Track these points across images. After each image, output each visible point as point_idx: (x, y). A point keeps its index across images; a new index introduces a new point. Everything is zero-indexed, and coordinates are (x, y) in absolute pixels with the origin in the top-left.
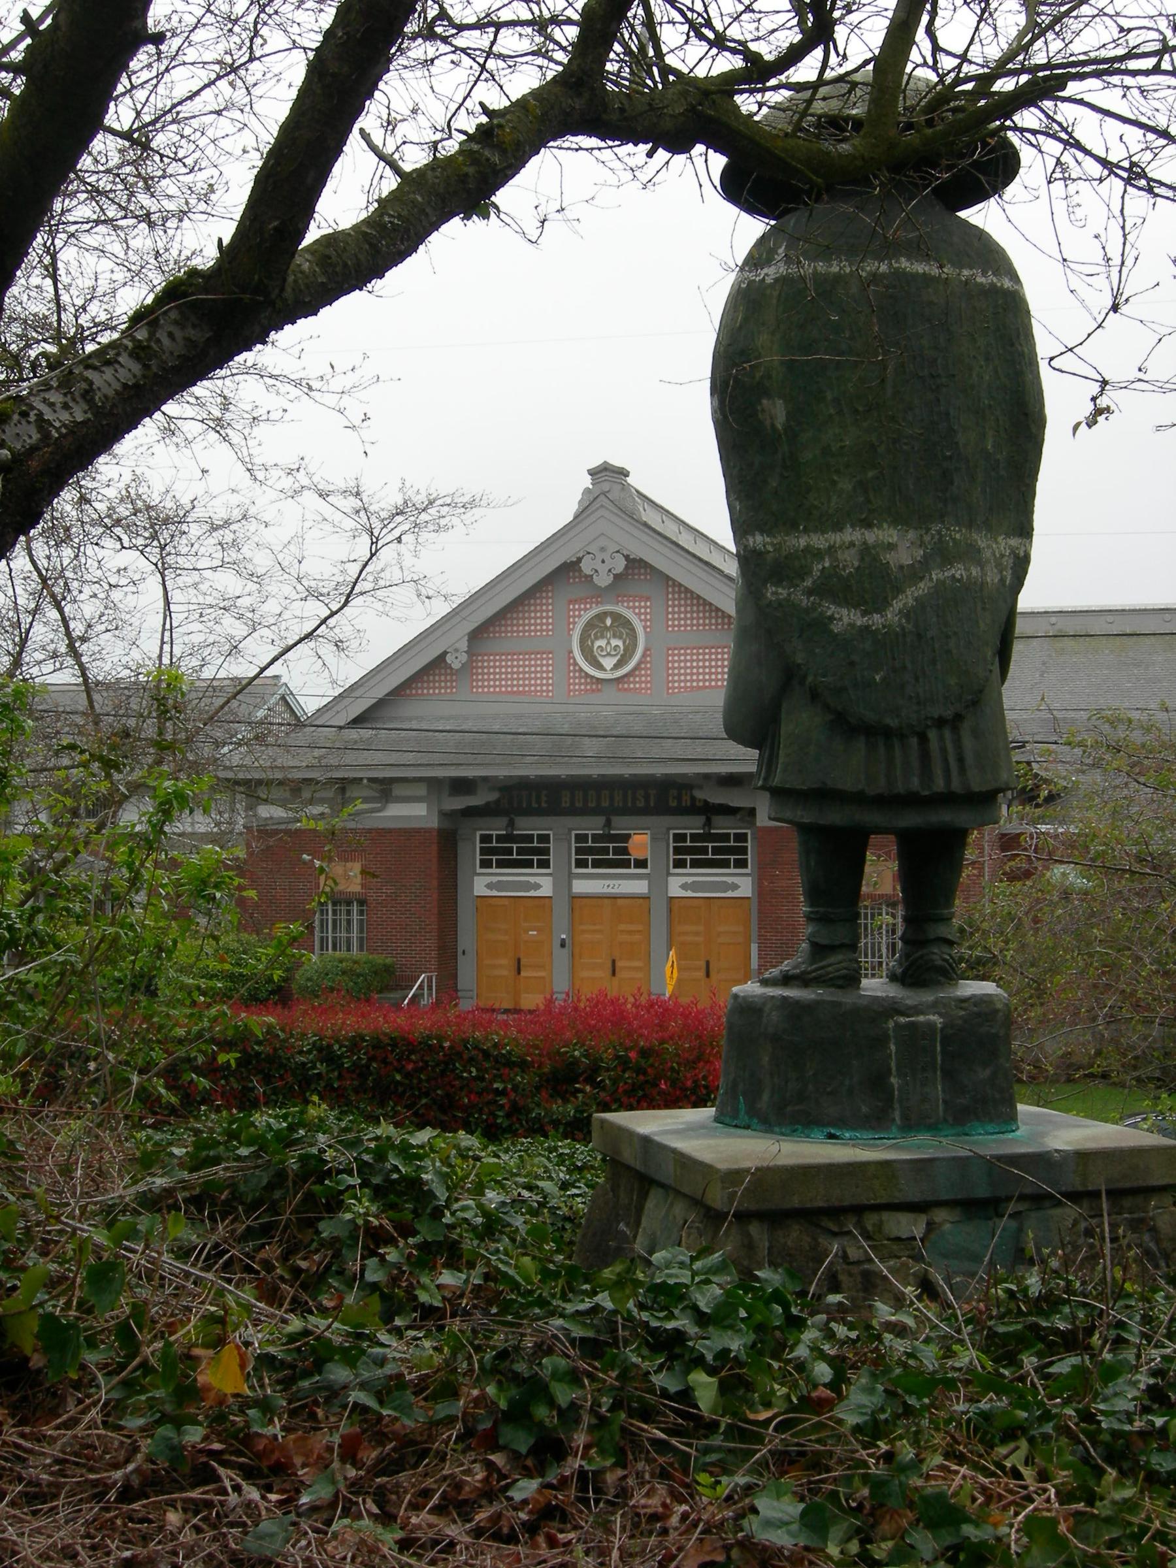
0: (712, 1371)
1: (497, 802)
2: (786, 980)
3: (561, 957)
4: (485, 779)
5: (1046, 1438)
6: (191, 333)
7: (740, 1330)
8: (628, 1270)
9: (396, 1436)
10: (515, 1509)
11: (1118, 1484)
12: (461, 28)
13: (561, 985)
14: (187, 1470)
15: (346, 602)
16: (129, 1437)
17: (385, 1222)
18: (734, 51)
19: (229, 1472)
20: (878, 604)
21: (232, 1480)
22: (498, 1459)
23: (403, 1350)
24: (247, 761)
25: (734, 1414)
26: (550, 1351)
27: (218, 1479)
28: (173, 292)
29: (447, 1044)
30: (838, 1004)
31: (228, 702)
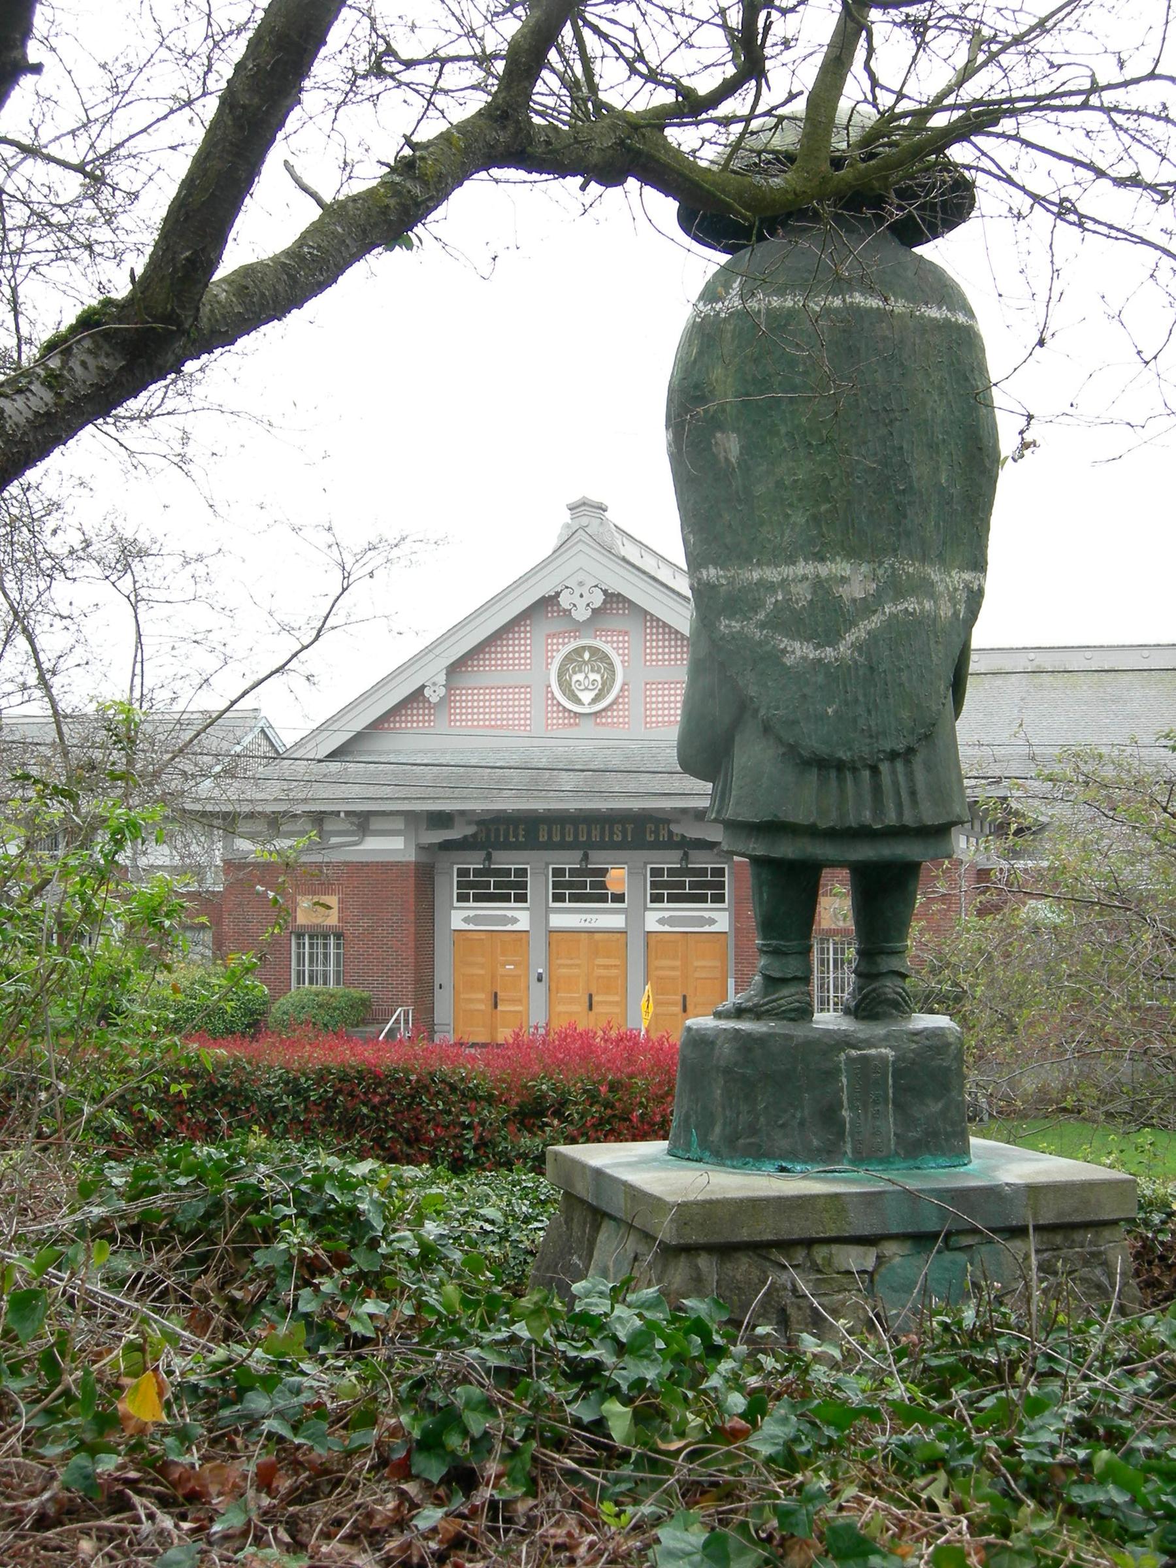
0: (627, 1401)
1: (474, 836)
2: (739, 1012)
3: (538, 992)
4: (462, 813)
5: (968, 1471)
6: (106, 362)
7: (655, 1360)
8: (546, 1300)
9: (311, 1466)
10: (426, 1538)
11: (1036, 1516)
12: (409, 64)
13: (537, 1017)
14: (100, 1498)
15: (318, 636)
16: (49, 1465)
17: (320, 1252)
18: (668, 86)
19: (145, 1501)
20: (831, 637)
21: (146, 1508)
22: (411, 1488)
23: (322, 1379)
24: (217, 792)
25: (645, 1444)
26: (466, 1380)
27: (132, 1507)
28: (87, 321)
29: (413, 1078)
30: (788, 1037)
31: (196, 736)
